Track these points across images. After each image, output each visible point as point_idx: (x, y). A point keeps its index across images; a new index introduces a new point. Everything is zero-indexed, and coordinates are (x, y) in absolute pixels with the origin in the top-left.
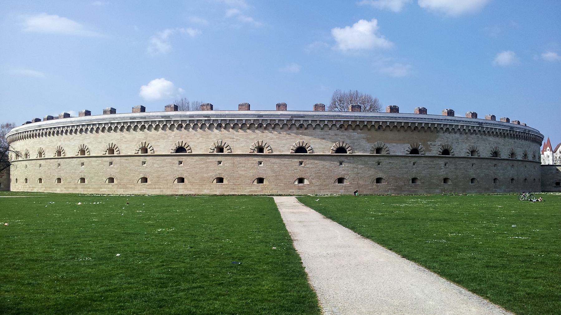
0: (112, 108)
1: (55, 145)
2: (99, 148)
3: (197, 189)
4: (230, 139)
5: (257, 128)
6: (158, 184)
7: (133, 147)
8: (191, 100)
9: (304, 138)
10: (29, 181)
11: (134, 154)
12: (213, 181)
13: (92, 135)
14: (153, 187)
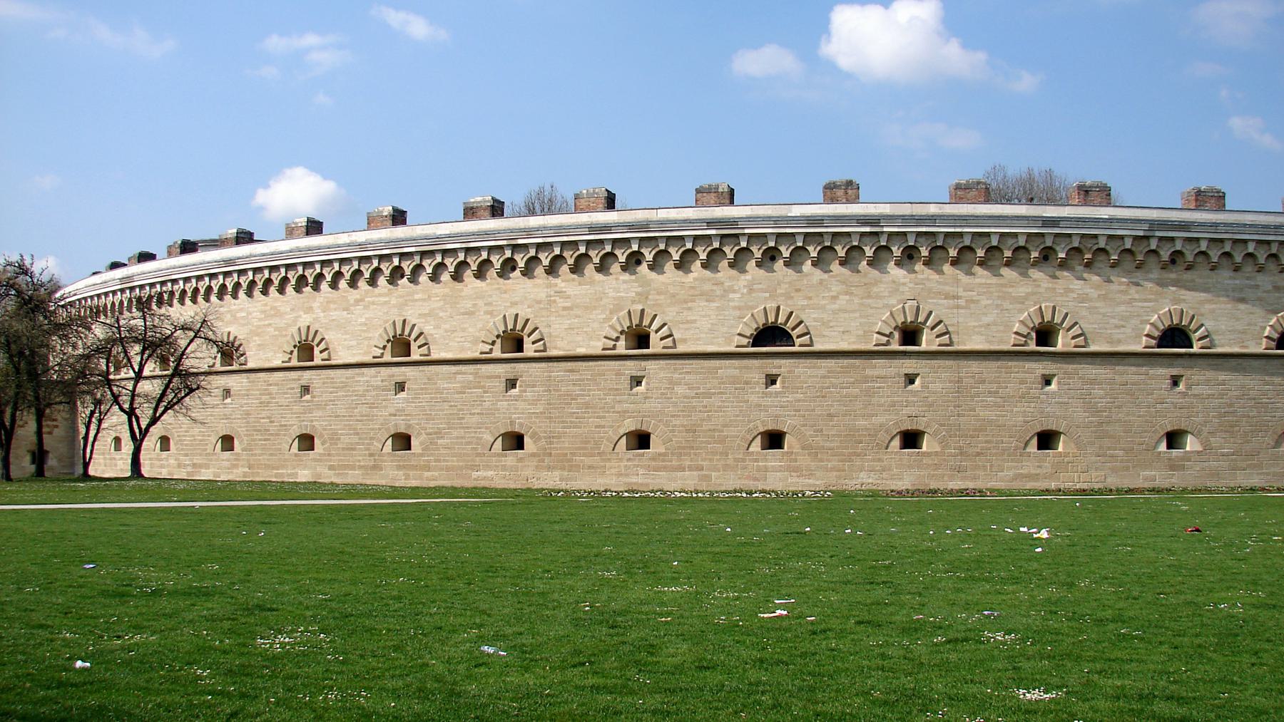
0: (395, 210)
1: (289, 325)
2: (464, 330)
3: (832, 469)
4: (945, 299)
5: (1035, 264)
6: (689, 454)
7: (596, 325)
8: (566, 192)
9: (1184, 300)
10: (175, 444)
11: (599, 352)
12: (890, 442)
13: (354, 295)
14: (674, 463)
